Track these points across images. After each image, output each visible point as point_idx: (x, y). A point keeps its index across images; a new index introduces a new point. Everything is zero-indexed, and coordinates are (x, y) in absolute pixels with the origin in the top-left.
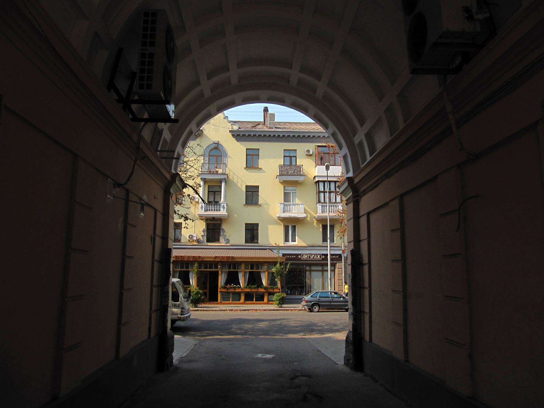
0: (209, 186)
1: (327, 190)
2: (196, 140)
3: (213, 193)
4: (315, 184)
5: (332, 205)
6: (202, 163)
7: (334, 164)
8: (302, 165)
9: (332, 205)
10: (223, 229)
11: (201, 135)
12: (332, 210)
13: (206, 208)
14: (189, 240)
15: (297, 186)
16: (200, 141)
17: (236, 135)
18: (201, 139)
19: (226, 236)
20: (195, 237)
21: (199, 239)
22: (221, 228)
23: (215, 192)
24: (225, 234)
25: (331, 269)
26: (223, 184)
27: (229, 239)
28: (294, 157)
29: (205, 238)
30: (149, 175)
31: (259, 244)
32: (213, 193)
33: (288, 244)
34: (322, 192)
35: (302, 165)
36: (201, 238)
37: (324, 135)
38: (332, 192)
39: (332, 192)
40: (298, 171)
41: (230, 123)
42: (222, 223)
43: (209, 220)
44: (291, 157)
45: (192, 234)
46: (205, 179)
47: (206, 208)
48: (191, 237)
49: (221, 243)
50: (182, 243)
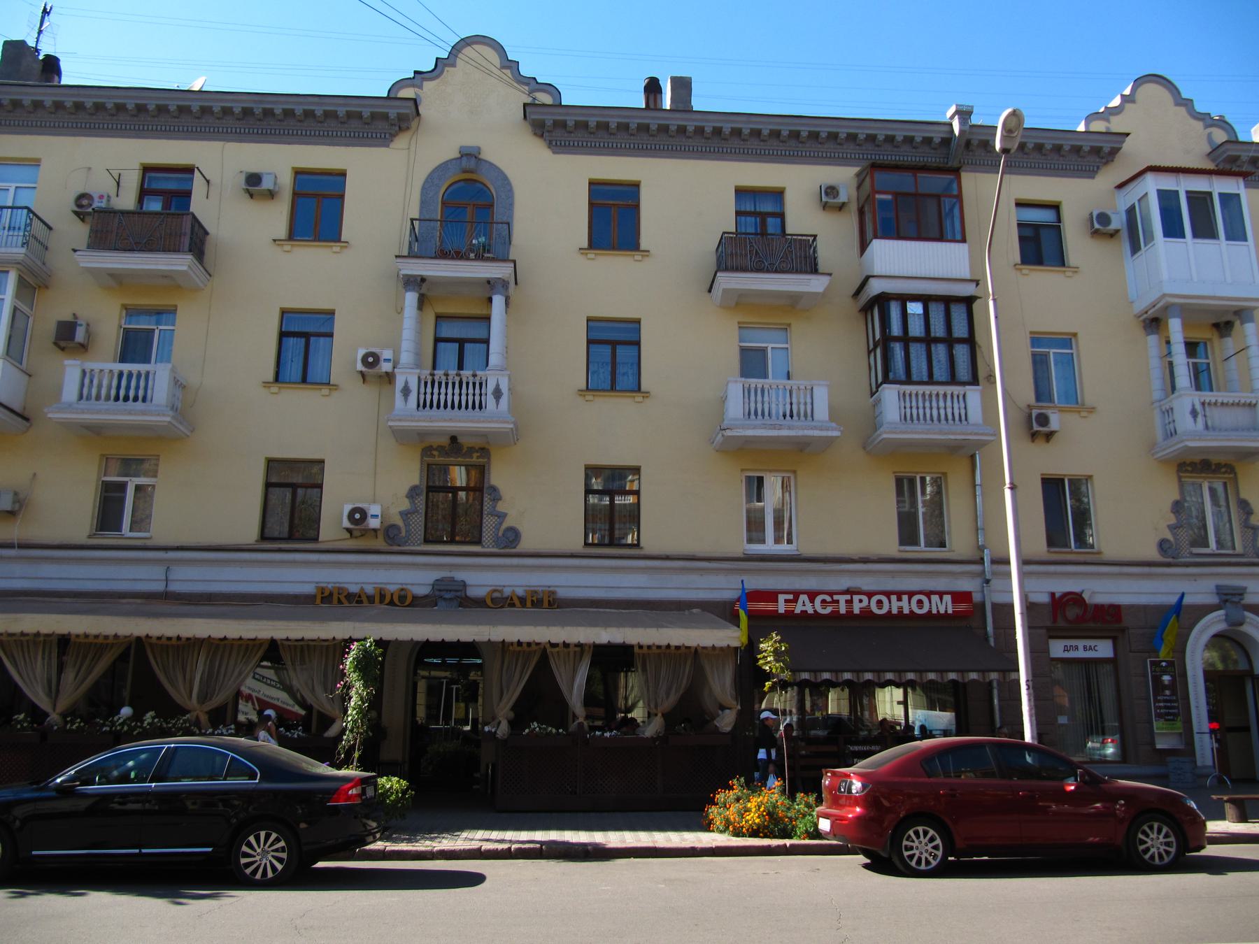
0: (439, 318)
1: (938, 330)
2: (392, 145)
3: (457, 345)
4: (861, 317)
5: (941, 393)
6: (412, 220)
7: (938, 236)
8: (815, 236)
9: (941, 393)
10: (494, 489)
11: (414, 124)
12: (942, 412)
13: (422, 397)
14: (348, 530)
15: (786, 328)
16: (409, 149)
17: (549, 123)
18: (413, 141)
19: (505, 515)
20: (375, 516)
21: (393, 526)
22: (486, 485)
23: (461, 342)
24: (501, 507)
25: (1016, 673)
26: (498, 300)
27: (517, 526)
28: (773, 215)
29: (418, 521)
30: (375, 473)
31: (642, 548)
32: (457, 345)
33: (911, 551)
34: (896, 339)
35: (815, 236)
36: (400, 523)
37: (890, 133)
38: (937, 340)
39: (937, 340)
40: (800, 257)
41: (527, 84)
42: (489, 462)
43: (435, 453)
44: (764, 216)
45: (360, 506)
46: (423, 280)
47: (422, 397)
48: (357, 516)
49: (483, 547)
50: (321, 542)
